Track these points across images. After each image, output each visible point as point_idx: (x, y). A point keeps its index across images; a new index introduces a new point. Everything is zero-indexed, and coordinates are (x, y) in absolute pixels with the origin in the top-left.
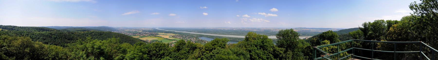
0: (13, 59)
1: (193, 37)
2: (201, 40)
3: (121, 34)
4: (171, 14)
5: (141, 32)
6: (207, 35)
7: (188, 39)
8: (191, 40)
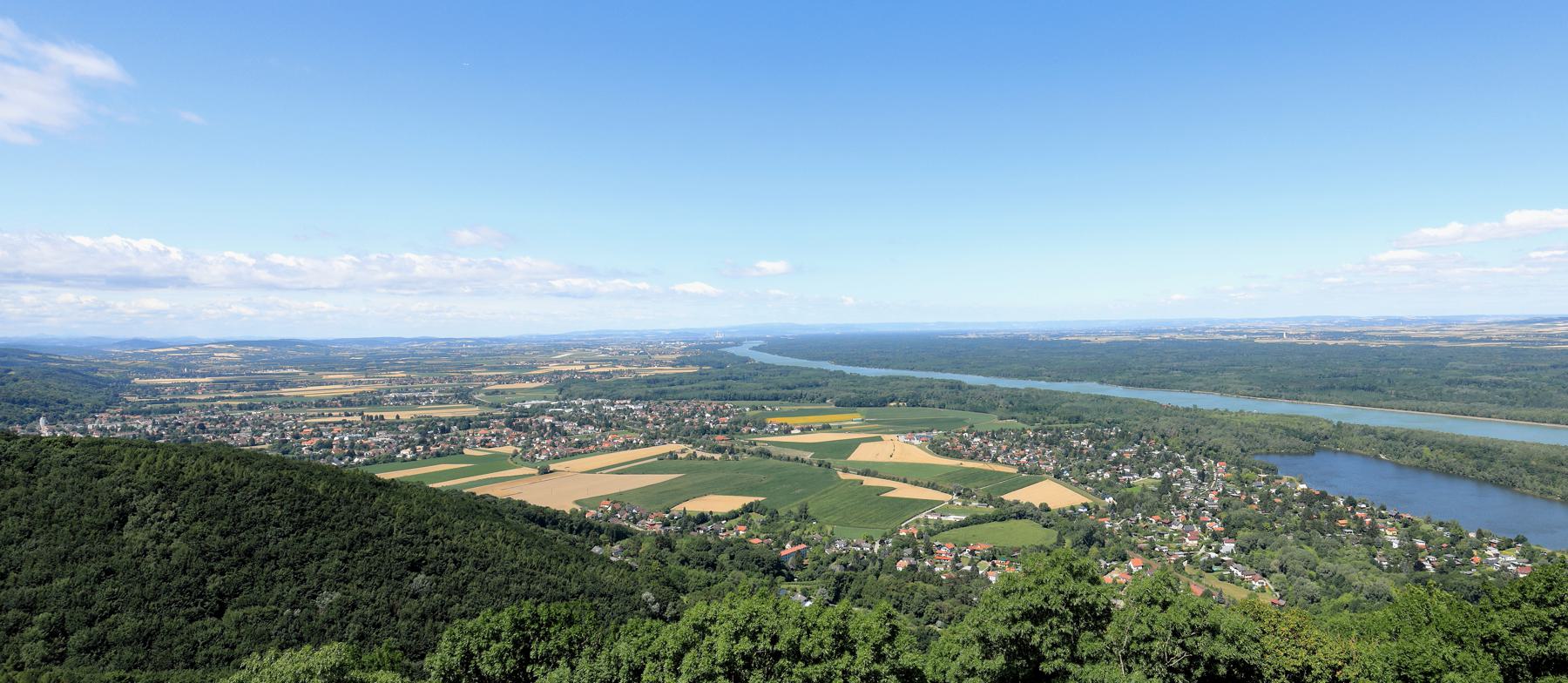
0: (4, 509)
1: (1201, 450)
2: (1307, 498)
3: (223, 454)
4: (763, 264)
5: (540, 410)
6: (1390, 436)
7: (1138, 480)
8: (1166, 484)
